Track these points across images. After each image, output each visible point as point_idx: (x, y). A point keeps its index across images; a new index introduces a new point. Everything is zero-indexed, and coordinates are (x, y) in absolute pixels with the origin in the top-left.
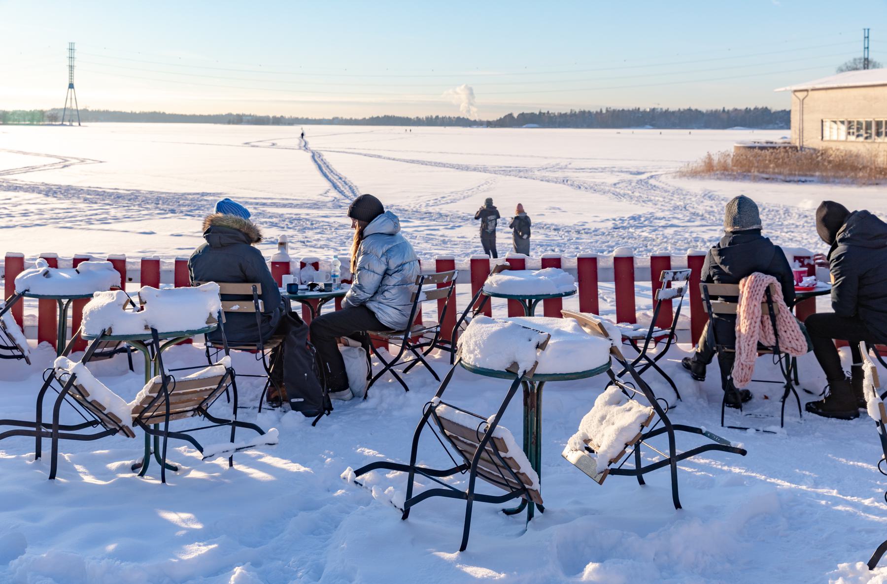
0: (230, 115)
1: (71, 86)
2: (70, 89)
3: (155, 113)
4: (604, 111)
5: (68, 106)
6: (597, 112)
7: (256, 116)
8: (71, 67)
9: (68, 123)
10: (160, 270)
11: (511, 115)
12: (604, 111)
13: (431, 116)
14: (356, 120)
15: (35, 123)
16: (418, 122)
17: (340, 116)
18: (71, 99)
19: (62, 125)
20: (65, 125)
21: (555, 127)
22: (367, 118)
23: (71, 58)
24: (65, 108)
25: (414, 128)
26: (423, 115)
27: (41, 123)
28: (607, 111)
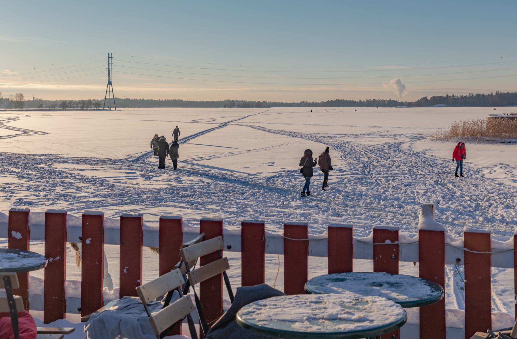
0: (227, 101)
1: (110, 83)
2: (109, 85)
3: (175, 100)
4: (494, 94)
5: (108, 97)
6: (489, 95)
7: (246, 102)
8: (110, 70)
9: (108, 109)
10: (29, 224)
11: (426, 98)
12: (494, 94)
13: (370, 99)
14: (317, 103)
15: (85, 109)
16: (361, 104)
17: (305, 101)
18: (110, 91)
19: (110, 110)
20: (106, 110)
21: (458, 106)
22: (325, 101)
23: (110, 63)
24: (105, 99)
25: (358, 109)
26: (364, 99)
27: (89, 109)
28: (497, 94)
